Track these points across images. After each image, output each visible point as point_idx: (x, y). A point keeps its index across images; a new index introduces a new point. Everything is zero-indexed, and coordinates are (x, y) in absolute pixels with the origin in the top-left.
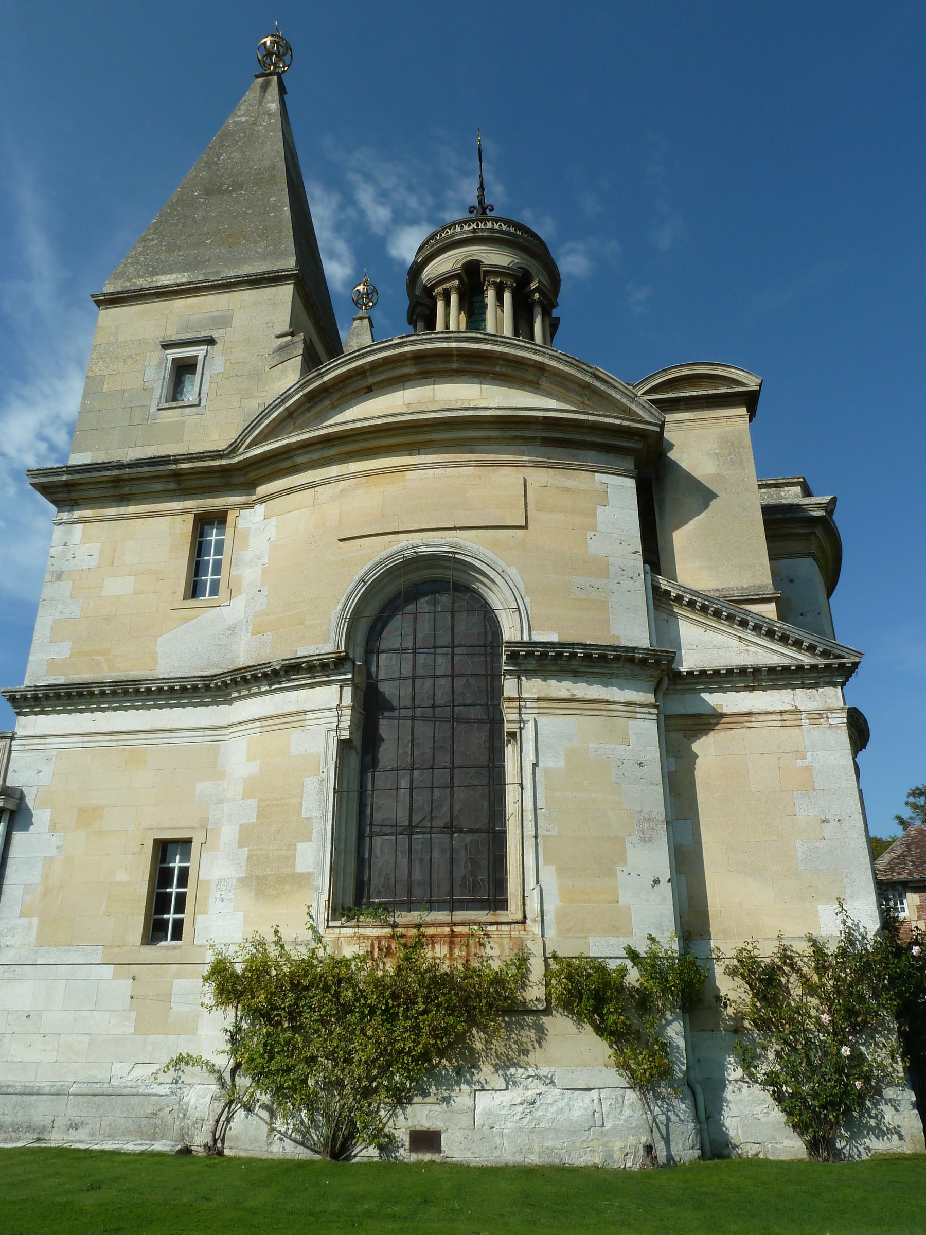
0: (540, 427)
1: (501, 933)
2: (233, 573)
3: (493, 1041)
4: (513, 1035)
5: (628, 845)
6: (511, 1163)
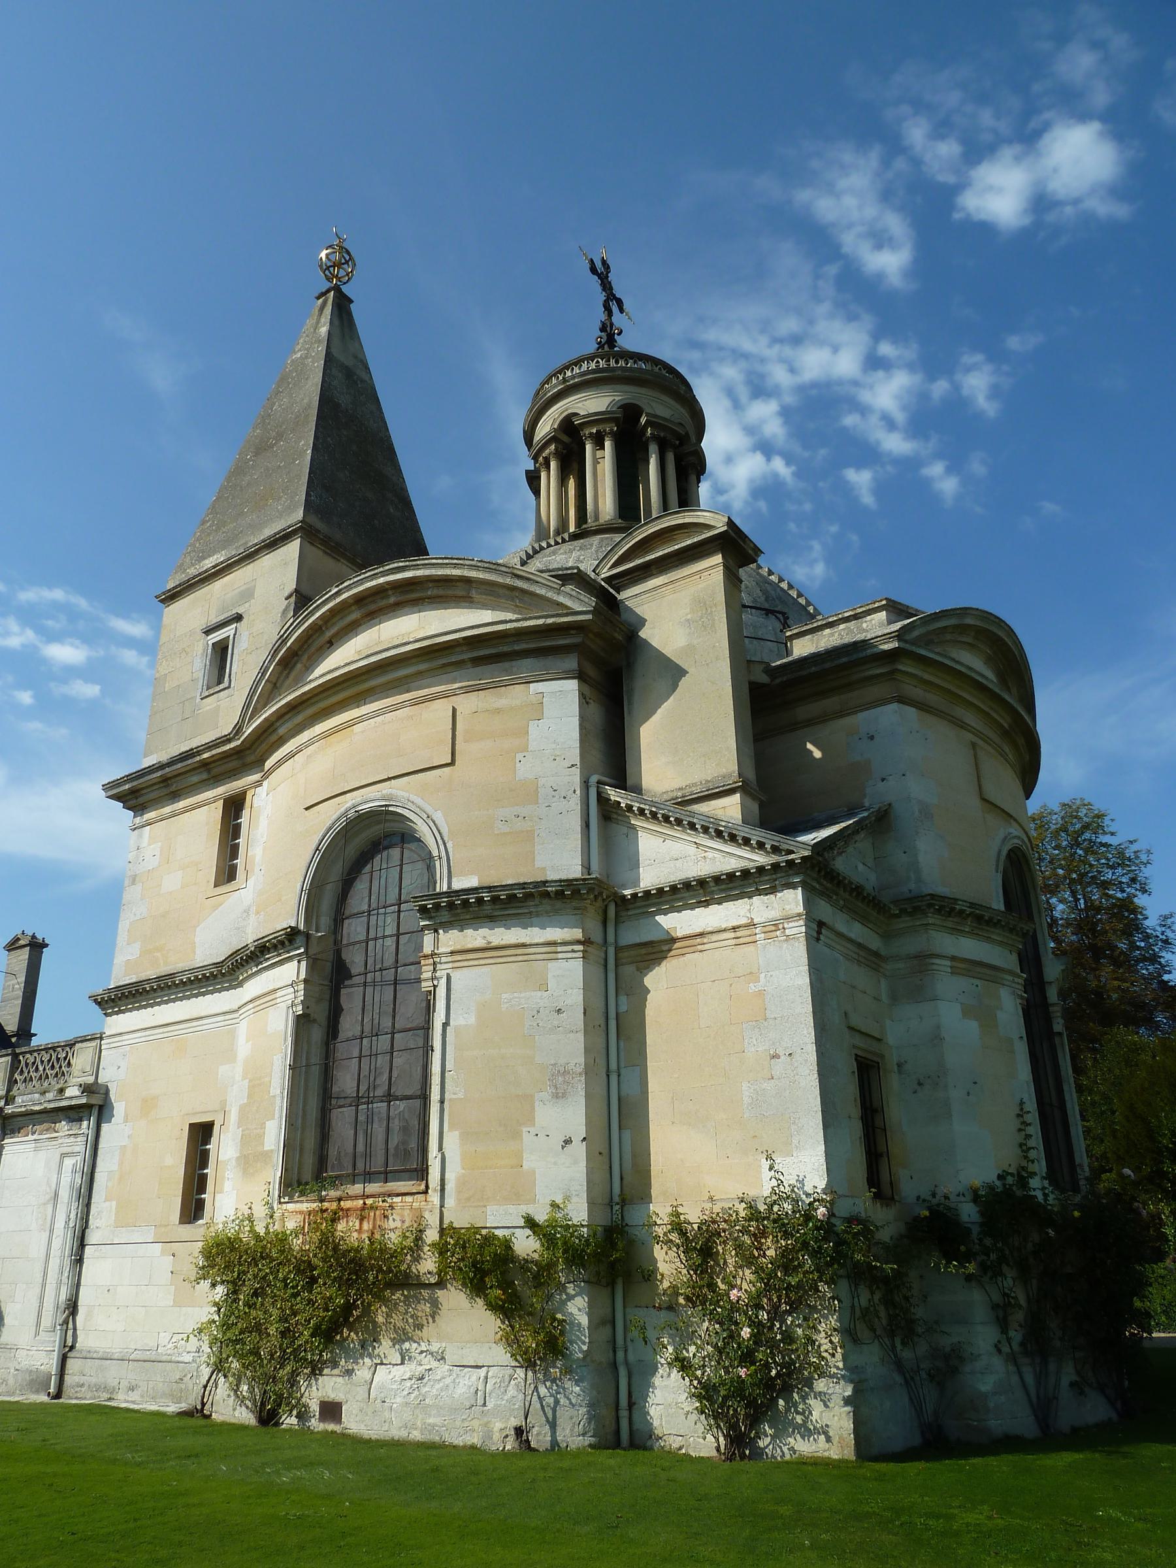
0: (464, 648)
1: (404, 1204)
3: (393, 1315)
4: (411, 1310)
5: (537, 1103)
6: (396, 1438)
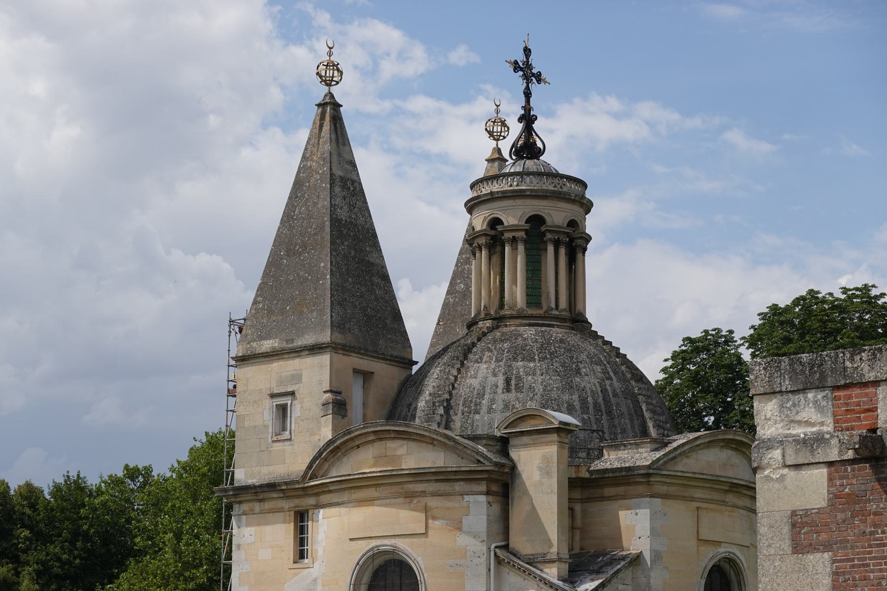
2: (313, 548)
